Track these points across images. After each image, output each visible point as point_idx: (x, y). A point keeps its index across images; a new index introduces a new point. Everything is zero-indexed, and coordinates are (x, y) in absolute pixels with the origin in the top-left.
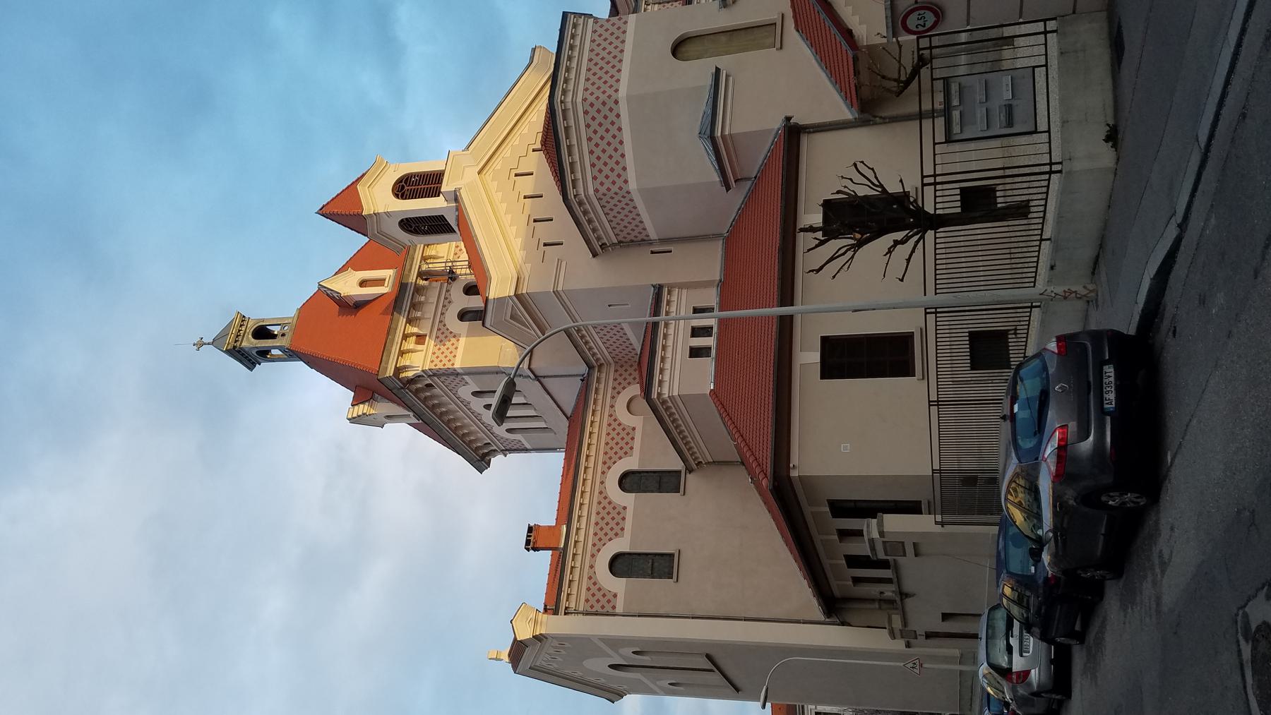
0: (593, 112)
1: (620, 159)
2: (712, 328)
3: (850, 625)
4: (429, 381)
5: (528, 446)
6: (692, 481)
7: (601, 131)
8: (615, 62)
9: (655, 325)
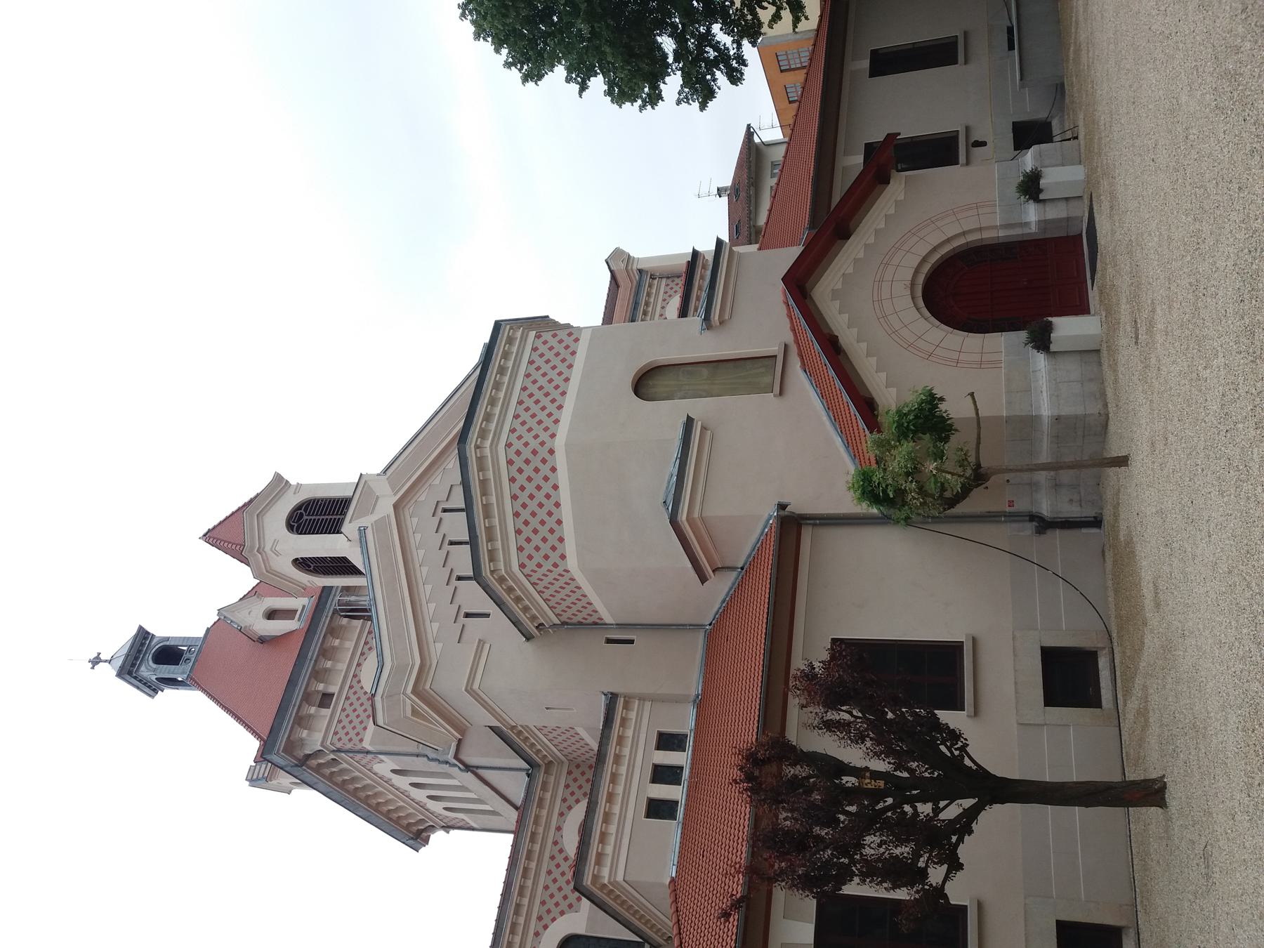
0: (519, 462)
1: (551, 492)
2: (681, 768)
5: (475, 825)
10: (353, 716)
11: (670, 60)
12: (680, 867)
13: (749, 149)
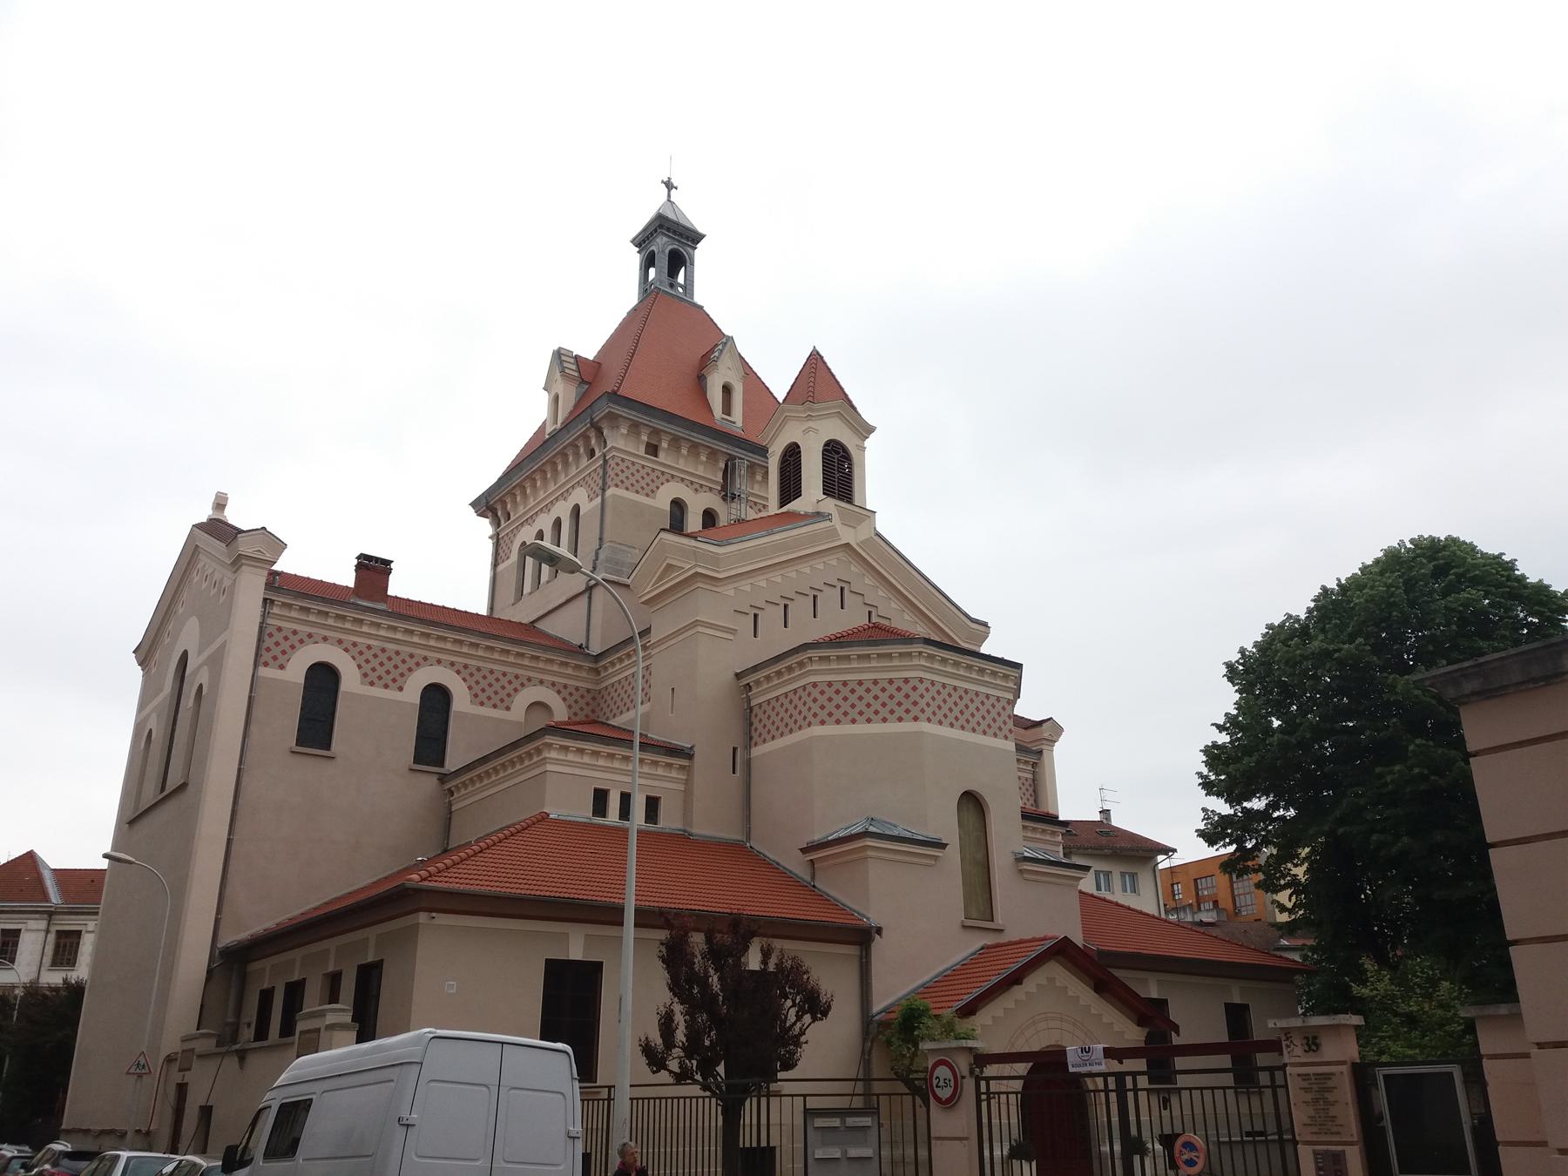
0: (906, 689)
1: (880, 716)
3: (208, 980)
4: (598, 454)
5: (500, 568)
6: (427, 784)
7: (884, 697)
8: (962, 721)
9: (629, 743)
10: (638, 476)
11: (1245, 804)
12: (558, 823)
13: (1151, 850)
